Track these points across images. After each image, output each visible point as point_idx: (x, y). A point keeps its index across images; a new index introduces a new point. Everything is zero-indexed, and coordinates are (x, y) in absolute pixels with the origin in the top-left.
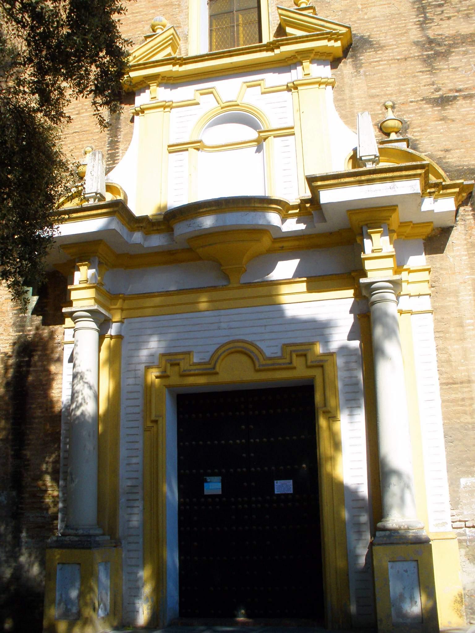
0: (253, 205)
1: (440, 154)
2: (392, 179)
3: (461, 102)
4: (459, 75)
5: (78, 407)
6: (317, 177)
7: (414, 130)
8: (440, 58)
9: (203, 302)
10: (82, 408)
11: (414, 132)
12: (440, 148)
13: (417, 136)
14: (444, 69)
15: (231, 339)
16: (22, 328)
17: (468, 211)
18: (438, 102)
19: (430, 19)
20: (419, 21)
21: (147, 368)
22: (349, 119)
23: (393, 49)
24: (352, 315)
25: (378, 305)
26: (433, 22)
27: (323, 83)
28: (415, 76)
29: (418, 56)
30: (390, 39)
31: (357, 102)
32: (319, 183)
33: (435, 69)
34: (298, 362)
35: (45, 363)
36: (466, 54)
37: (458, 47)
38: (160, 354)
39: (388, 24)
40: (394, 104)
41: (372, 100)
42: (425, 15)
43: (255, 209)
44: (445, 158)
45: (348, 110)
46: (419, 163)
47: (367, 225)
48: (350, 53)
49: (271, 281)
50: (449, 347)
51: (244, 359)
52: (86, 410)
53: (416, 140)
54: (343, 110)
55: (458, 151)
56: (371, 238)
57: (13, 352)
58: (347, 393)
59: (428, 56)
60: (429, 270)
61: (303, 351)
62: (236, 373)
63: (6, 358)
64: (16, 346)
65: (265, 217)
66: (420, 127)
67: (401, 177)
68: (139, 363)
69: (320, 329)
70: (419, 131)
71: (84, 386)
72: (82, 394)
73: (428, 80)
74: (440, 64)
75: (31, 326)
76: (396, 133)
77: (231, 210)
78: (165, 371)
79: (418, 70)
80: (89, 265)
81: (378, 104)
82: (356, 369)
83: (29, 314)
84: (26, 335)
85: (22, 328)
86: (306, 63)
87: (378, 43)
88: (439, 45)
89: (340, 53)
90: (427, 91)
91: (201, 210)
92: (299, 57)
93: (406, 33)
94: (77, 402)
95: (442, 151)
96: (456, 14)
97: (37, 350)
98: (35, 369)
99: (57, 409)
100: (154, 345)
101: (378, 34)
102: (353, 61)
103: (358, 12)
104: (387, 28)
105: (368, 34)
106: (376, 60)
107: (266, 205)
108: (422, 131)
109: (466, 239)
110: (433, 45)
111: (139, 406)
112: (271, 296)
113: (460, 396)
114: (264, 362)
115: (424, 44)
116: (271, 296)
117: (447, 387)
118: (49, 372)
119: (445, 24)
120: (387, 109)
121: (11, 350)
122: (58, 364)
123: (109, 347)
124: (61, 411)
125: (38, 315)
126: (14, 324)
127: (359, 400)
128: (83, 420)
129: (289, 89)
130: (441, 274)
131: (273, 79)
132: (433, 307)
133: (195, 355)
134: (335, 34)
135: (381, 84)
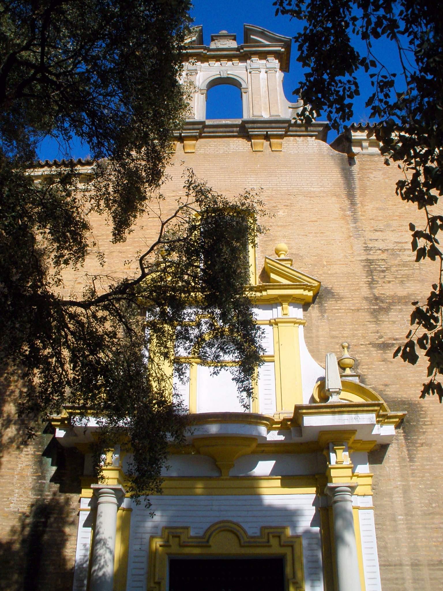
0: (250, 420)
1: (381, 387)
2: (357, 412)
4: (396, 327)
5: (100, 569)
6: (303, 406)
7: (363, 367)
9: (199, 488)
10: (104, 570)
11: (363, 369)
13: (364, 372)
15: (221, 519)
16: (41, 493)
17: (400, 433)
18: (380, 347)
19: (376, 281)
20: (368, 281)
21: (152, 537)
22: (316, 353)
23: (349, 301)
24: (314, 507)
25: (339, 503)
26: (378, 283)
28: (364, 325)
29: (368, 309)
30: (347, 292)
31: (322, 340)
32: (304, 411)
33: (380, 321)
34: (274, 542)
35: (60, 525)
36: (401, 312)
38: (163, 527)
39: (345, 280)
40: (349, 345)
41: (333, 340)
42: (372, 277)
43: (250, 423)
45: (315, 346)
46: (376, 402)
47: (333, 442)
48: (317, 300)
49: (254, 476)
50: (386, 536)
51: (231, 536)
52: (107, 571)
53: (365, 375)
54: (311, 345)
55: (394, 386)
56: (336, 453)
57: (30, 513)
58: (310, 568)
59: (374, 309)
60: (371, 476)
61: (277, 533)
62: (224, 547)
63: (23, 518)
64: (34, 508)
65: (257, 430)
66: (367, 365)
67: (363, 411)
68: (144, 533)
69: (290, 515)
70: (366, 369)
71: (106, 551)
72: (104, 558)
73: (374, 329)
74: (382, 317)
75: (49, 491)
76: (350, 368)
77: (234, 422)
78: (167, 541)
79: (367, 320)
81: (338, 343)
82: (317, 550)
83: (47, 481)
84: (44, 499)
85: (41, 493)
86: (285, 305)
87: (338, 294)
88: (382, 302)
89: (311, 300)
90: (373, 337)
92: (280, 300)
93: (358, 289)
94: (100, 564)
95: (383, 385)
96: (394, 279)
97: (54, 513)
98: (50, 529)
99: (70, 565)
101: (338, 289)
102: (319, 307)
103: (324, 266)
104: (344, 283)
105: (331, 286)
106: (336, 308)
107: (259, 421)
108: (369, 369)
110: (378, 301)
111: (143, 569)
112: (254, 488)
113: (394, 575)
114: (248, 540)
116: (254, 488)
117: (384, 568)
118: (63, 533)
119: (387, 286)
120: (344, 348)
121: (29, 511)
122: (72, 527)
124: (74, 568)
125: (56, 483)
126: (33, 488)
127: (319, 574)
128: (104, 580)
130: (380, 480)
132: (374, 505)
134: (309, 286)
135: (340, 328)
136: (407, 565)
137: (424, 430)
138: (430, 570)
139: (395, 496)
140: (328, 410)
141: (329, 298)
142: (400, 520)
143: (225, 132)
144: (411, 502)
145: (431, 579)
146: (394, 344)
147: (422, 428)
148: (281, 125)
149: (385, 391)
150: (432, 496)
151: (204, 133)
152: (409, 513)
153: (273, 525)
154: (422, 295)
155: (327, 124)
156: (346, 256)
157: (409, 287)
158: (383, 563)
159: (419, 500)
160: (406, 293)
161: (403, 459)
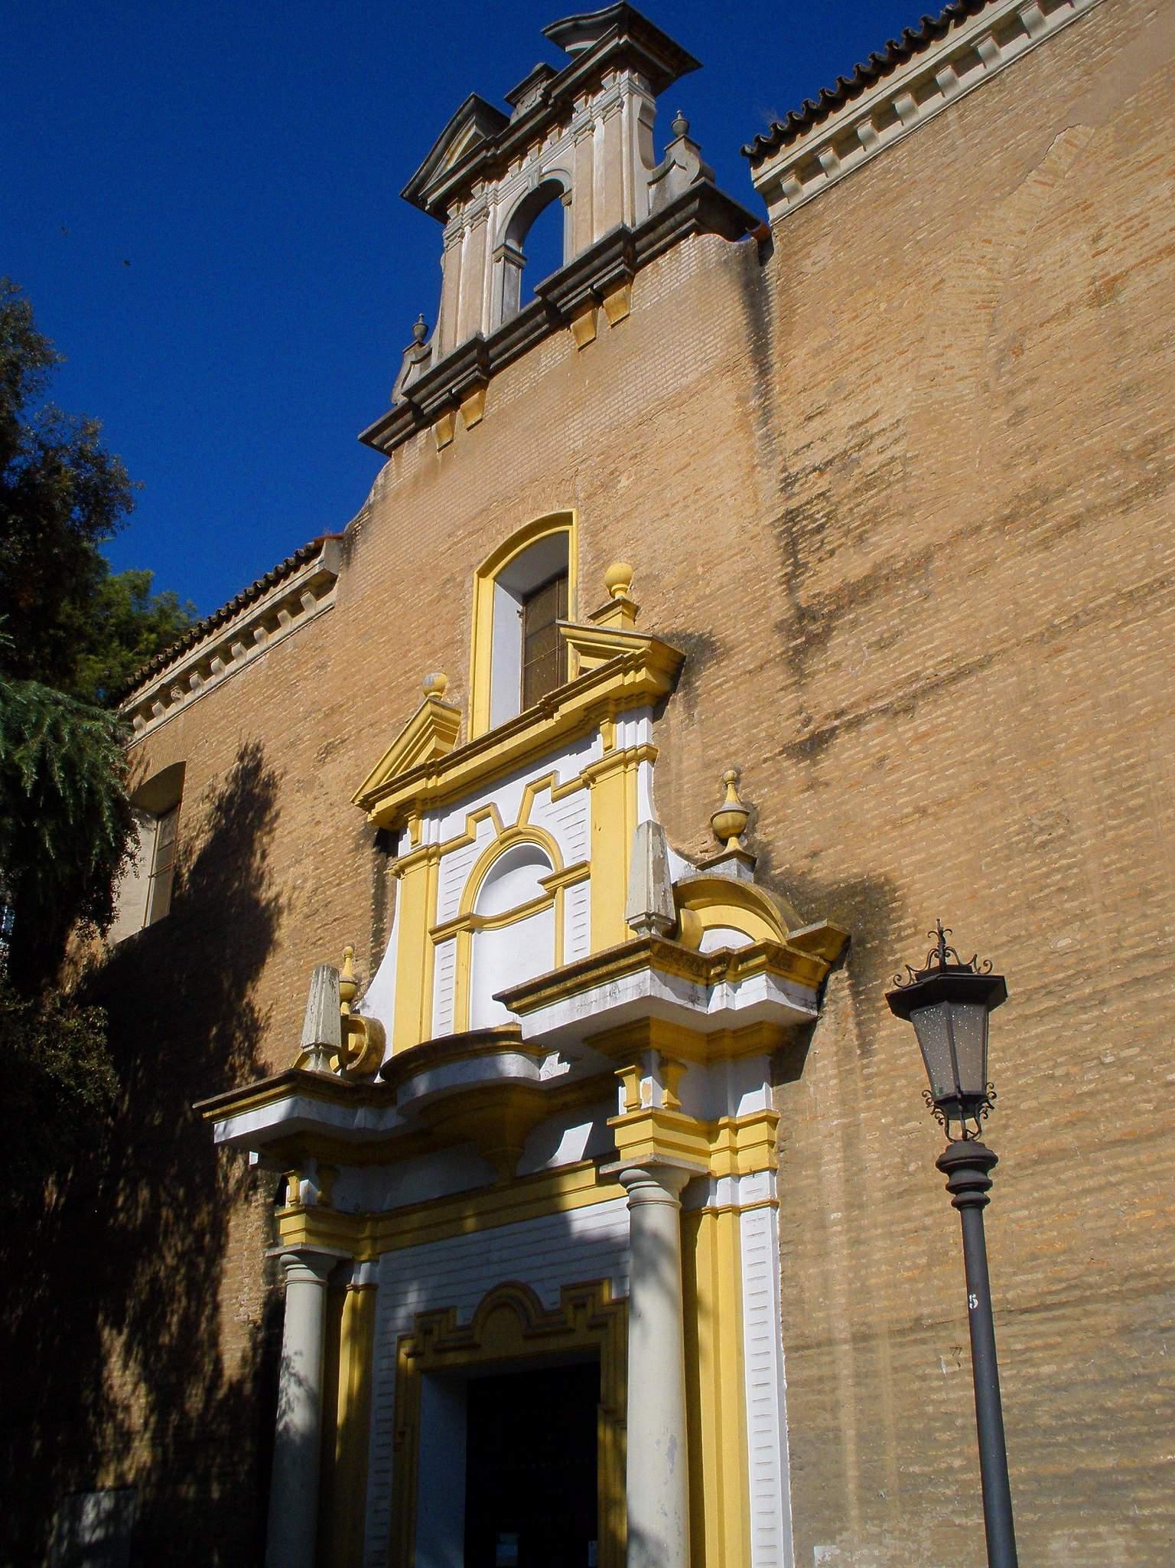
3: (843, 738)
8: (813, 649)
11: (767, 826)
12: (805, 853)
14: (821, 671)
17: (841, 981)
27: (631, 760)
28: (773, 702)
36: (855, 627)
37: (843, 615)
43: (476, 1054)
44: (810, 871)
53: (769, 843)
55: (831, 851)
59: (797, 650)
76: (738, 836)
80: (639, 1070)
91: (412, 1066)
93: (765, 608)
95: (806, 857)
100: (413, 1300)
107: (489, 1045)
109: (836, 1042)
113: (814, 1372)
115: (792, 625)
117: (797, 1355)
119: (824, 568)
123: (354, 1309)
129: (586, 784)
131: (568, 767)
133: (459, 1313)
136: (846, 1342)
137: (898, 956)
138: (893, 1346)
139: (826, 1159)
140: (554, 989)
141: (705, 663)
142: (836, 1223)
143: (526, 336)
144: (861, 1170)
145: (895, 1370)
146: (836, 727)
147: (893, 952)
148: (611, 253)
149: (810, 871)
150: (910, 1141)
151: (493, 361)
152: (854, 1203)
153: (580, 1279)
154: (906, 554)
155: (104, 914)
156: (743, 529)
157: (877, 546)
158: (791, 1343)
159: (878, 1159)
160: (869, 565)
161: (847, 1052)
